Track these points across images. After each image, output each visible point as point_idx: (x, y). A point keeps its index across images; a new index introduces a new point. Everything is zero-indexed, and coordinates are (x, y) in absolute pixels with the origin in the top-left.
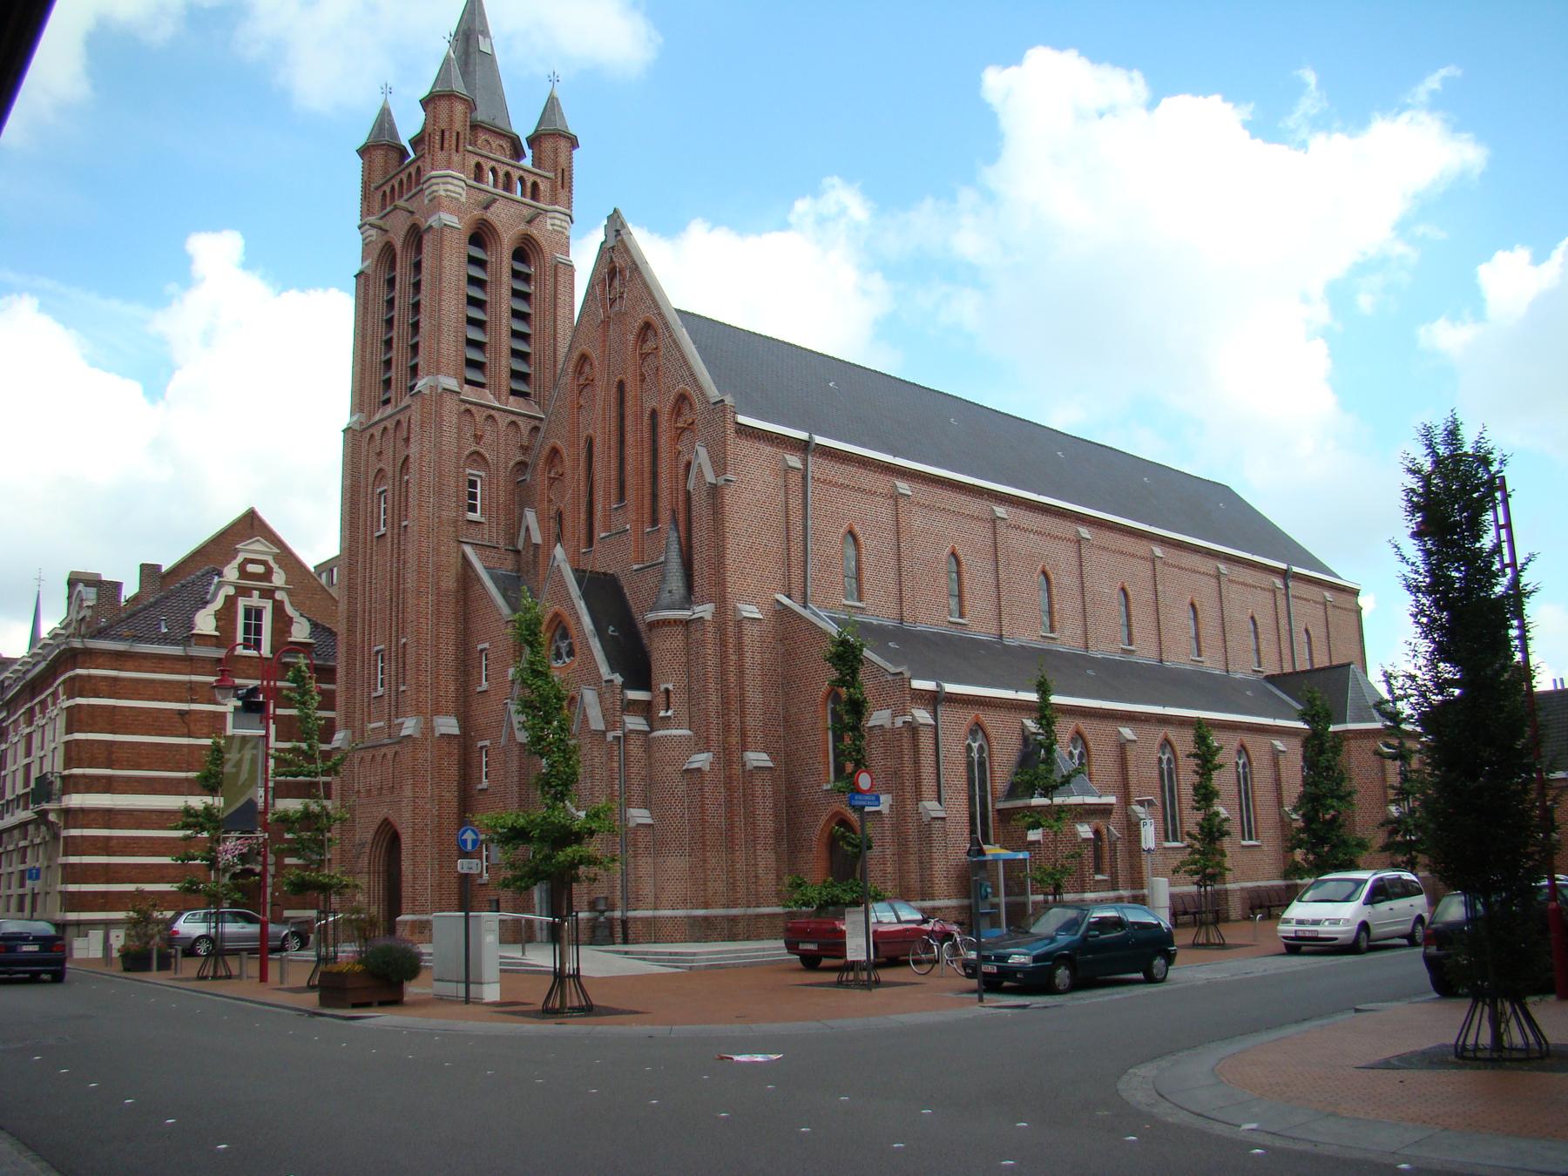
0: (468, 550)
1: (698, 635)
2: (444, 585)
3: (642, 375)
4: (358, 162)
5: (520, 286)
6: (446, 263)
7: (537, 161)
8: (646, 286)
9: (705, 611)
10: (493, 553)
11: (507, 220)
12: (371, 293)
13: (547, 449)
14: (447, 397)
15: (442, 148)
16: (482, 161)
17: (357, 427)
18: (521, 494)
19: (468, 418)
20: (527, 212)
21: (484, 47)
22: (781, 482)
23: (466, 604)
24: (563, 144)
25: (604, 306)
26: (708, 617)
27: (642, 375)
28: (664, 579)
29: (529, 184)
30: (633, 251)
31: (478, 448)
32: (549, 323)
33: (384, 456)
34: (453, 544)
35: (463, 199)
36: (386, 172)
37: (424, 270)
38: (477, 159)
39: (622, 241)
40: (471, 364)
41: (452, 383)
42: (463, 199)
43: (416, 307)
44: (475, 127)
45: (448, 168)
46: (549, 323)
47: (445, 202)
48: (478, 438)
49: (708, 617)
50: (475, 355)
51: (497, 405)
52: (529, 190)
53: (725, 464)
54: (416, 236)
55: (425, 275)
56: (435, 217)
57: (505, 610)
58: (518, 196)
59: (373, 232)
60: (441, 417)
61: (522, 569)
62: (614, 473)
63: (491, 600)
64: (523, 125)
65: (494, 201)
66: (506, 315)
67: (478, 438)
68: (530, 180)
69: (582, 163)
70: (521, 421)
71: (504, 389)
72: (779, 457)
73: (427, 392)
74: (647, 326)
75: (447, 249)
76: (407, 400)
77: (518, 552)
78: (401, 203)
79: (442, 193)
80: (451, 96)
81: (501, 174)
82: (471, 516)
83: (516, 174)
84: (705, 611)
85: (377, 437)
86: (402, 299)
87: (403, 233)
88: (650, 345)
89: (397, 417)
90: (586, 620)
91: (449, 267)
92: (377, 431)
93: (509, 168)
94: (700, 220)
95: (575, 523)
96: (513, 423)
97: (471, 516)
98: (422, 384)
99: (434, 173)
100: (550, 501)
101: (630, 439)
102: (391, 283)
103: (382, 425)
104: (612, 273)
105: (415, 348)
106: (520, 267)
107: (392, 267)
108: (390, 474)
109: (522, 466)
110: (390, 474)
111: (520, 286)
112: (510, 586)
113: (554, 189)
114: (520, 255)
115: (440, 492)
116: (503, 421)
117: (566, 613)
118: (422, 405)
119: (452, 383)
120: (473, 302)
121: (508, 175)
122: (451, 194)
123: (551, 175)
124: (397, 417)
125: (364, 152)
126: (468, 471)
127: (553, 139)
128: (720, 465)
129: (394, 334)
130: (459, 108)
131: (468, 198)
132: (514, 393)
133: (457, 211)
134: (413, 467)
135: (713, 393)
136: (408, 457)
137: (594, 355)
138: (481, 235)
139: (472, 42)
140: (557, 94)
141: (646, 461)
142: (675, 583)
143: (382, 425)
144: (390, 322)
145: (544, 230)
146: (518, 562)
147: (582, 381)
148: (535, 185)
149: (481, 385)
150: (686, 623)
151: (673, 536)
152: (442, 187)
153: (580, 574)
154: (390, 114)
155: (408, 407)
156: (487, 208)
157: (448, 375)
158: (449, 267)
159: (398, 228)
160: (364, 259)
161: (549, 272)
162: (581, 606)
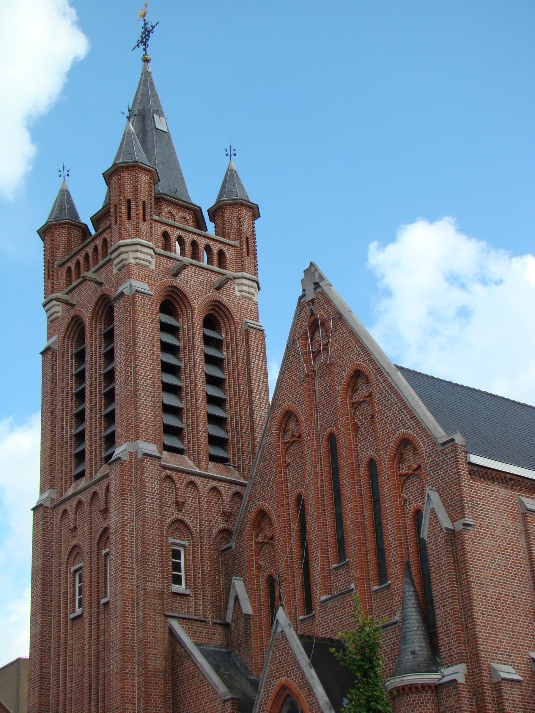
0: (175, 624)
1: (451, 701)
2: (151, 665)
3: (355, 425)
4: (38, 246)
5: (213, 352)
6: (139, 329)
7: (221, 230)
8: (353, 334)
9: (457, 672)
10: (201, 627)
11: (196, 285)
12: (59, 368)
13: (253, 512)
14: (148, 462)
15: (129, 218)
16: (169, 230)
17: (48, 504)
18: (227, 562)
19: (168, 484)
20: (215, 279)
21: (160, 124)
22: (520, 526)
23: (174, 685)
24: (246, 214)
25: (307, 360)
26: (461, 679)
27: (355, 425)
28: (403, 639)
29: (215, 252)
30: (336, 302)
31: (180, 516)
32: (243, 387)
33: (79, 531)
34: (162, 618)
35: (153, 267)
36: (69, 250)
37: (117, 338)
38: (164, 228)
39: (323, 293)
40: (169, 430)
41: (152, 449)
42: (153, 267)
43: (110, 376)
44: (159, 199)
45: (137, 236)
46: (243, 387)
47: (136, 270)
48: (180, 505)
49: (461, 679)
50: (172, 421)
51: (197, 470)
52: (215, 258)
53: (462, 507)
54: (106, 307)
55: (119, 343)
56: (127, 284)
57: (222, 688)
58: (205, 264)
59: (59, 308)
60: (143, 484)
61: (233, 648)
62: (330, 532)
63: (205, 678)
64: (204, 197)
65: (184, 267)
66: (201, 380)
67: (180, 505)
68: (216, 248)
69: (266, 233)
70: (222, 487)
71: (204, 455)
72: (515, 500)
73: (126, 458)
74: (358, 374)
75: (140, 316)
76: (104, 470)
77: (226, 625)
78: (89, 274)
79: (132, 261)
80: (134, 167)
81: (188, 243)
82: (176, 588)
83: (202, 243)
84: (457, 672)
85: (71, 513)
86: (94, 368)
87: (92, 304)
88: (362, 392)
89: (93, 489)
90: (319, 690)
91: (143, 332)
92: (70, 506)
93: (195, 237)
94: (452, 220)
95: (291, 587)
96: (215, 489)
97: (176, 588)
98: (119, 451)
99: (122, 242)
100: (259, 567)
101: (346, 491)
102: (80, 356)
103: (76, 500)
104: (314, 326)
105: (110, 418)
106: (210, 333)
107: (81, 339)
108: (86, 550)
109: (226, 533)
110: (86, 550)
111: (213, 352)
112: (223, 660)
113: (240, 257)
114: (210, 322)
115: (144, 561)
116: (204, 486)
117: (294, 685)
118: (123, 471)
119: (152, 449)
120: (167, 368)
121: (194, 244)
122: (141, 263)
123: (236, 243)
124: (93, 489)
125: (44, 233)
126: (171, 540)
127: (234, 209)
128: (456, 508)
129: (87, 405)
130: (144, 179)
131: (157, 266)
132: (213, 458)
133: (147, 278)
134: (114, 537)
135: (440, 434)
136: (106, 529)
137: (301, 411)
138: (172, 302)
139: (148, 121)
140: (234, 167)
141: (367, 513)
142: (416, 642)
143: (76, 500)
144: (80, 396)
145: (235, 294)
146: (227, 637)
147: (287, 438)
148: (221, 253)
149: (180, 451)
150: (436, 689)
151: (409, 591)
152: (131, 255)
153: (307, 640)
154: (69, 195)
155: (107, 476)
156: (176, 275)
157: (147, 440)
158: (143, 332)
159: (86, 300)
160: (49, 337)
161: (241, 337)
162: (312, 675)
